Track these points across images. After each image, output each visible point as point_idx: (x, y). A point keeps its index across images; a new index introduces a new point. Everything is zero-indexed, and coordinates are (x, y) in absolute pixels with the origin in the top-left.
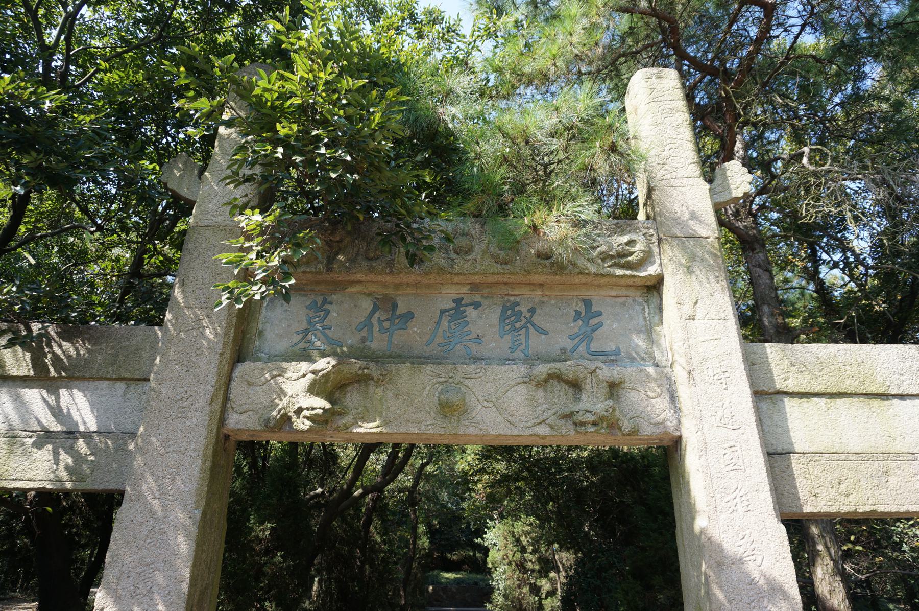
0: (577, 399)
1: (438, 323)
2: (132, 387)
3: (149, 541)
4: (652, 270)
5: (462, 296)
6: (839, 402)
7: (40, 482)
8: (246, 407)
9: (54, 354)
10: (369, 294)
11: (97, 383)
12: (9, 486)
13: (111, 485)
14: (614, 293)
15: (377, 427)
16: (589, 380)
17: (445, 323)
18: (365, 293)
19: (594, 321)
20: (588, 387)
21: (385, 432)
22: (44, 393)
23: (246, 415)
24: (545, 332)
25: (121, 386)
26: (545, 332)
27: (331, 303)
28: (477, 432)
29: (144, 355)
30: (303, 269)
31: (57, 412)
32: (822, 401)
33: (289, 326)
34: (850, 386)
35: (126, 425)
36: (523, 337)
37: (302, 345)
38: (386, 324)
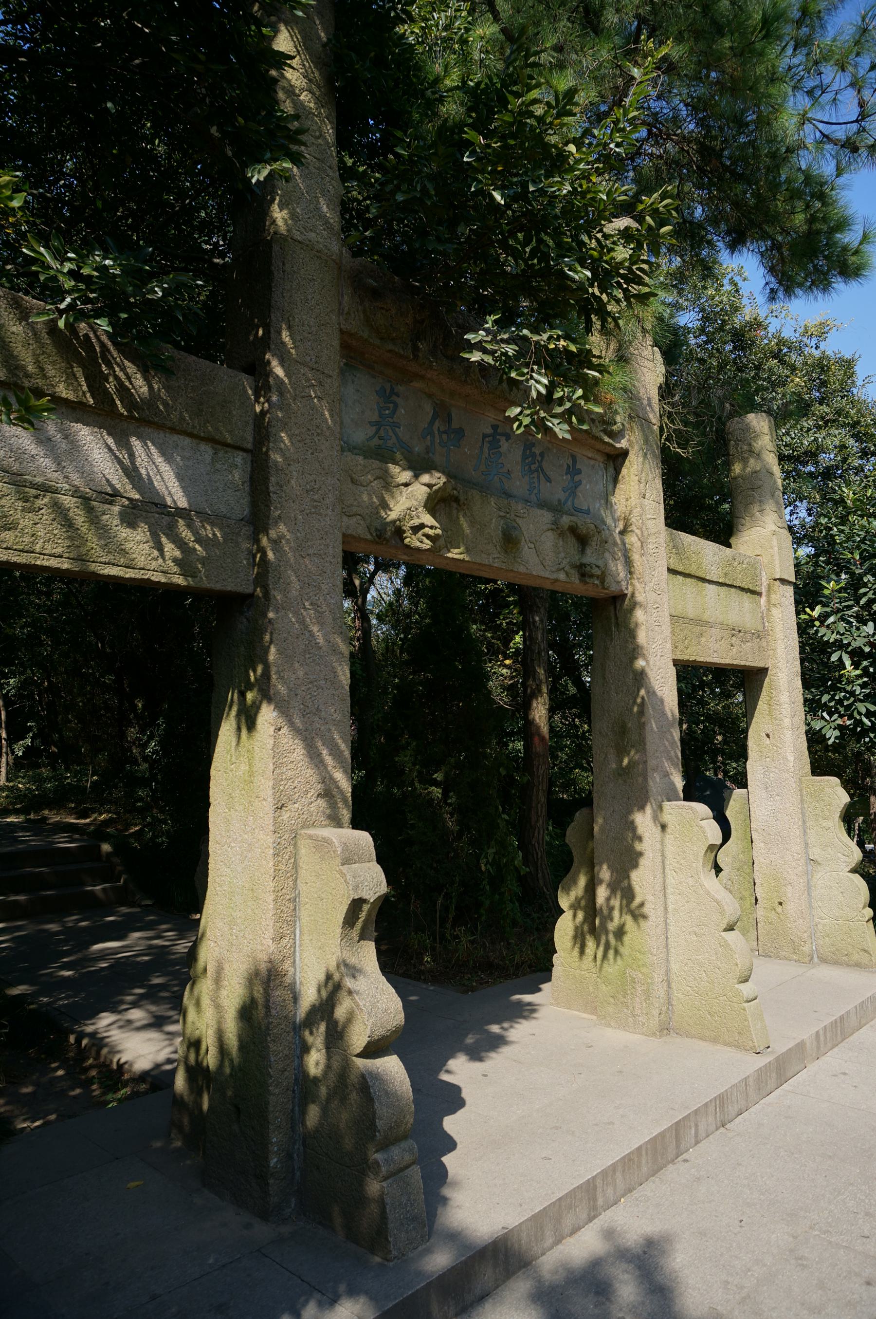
0: (583, 551)
1: (482, 448)
2: (221, 454)
3: (307, 656)
4: (623, 444)
5: (499, 423)
6: (688, 580)
7: (142, 572)
8: (355, 509)
9: (117, 378)
10: (430, 396)
11: (175, 437)
12: (102, 572)
13: (758, 664)
14: (590, 455)
15: (461, 553)
16: (595, 538)
17: (486, 445)
18: (425, 393)
19: (577, 478)
20: (594, 544)
21: (467, 559)
22: (110, 441)
23: (354, 519)
24: (549, 480)
25: (206, 450)
26: (549, 480)
27: (398, 396)
28: (525, 571)
29: (234, 413)
30: (391, 347)
31: (131, 473)
32: (680, 578)
33: (363, 412)
34: (693, 570)
35: (221, 506)
36: (536, 480)
37: (376, 441)
38: (445, 436)
